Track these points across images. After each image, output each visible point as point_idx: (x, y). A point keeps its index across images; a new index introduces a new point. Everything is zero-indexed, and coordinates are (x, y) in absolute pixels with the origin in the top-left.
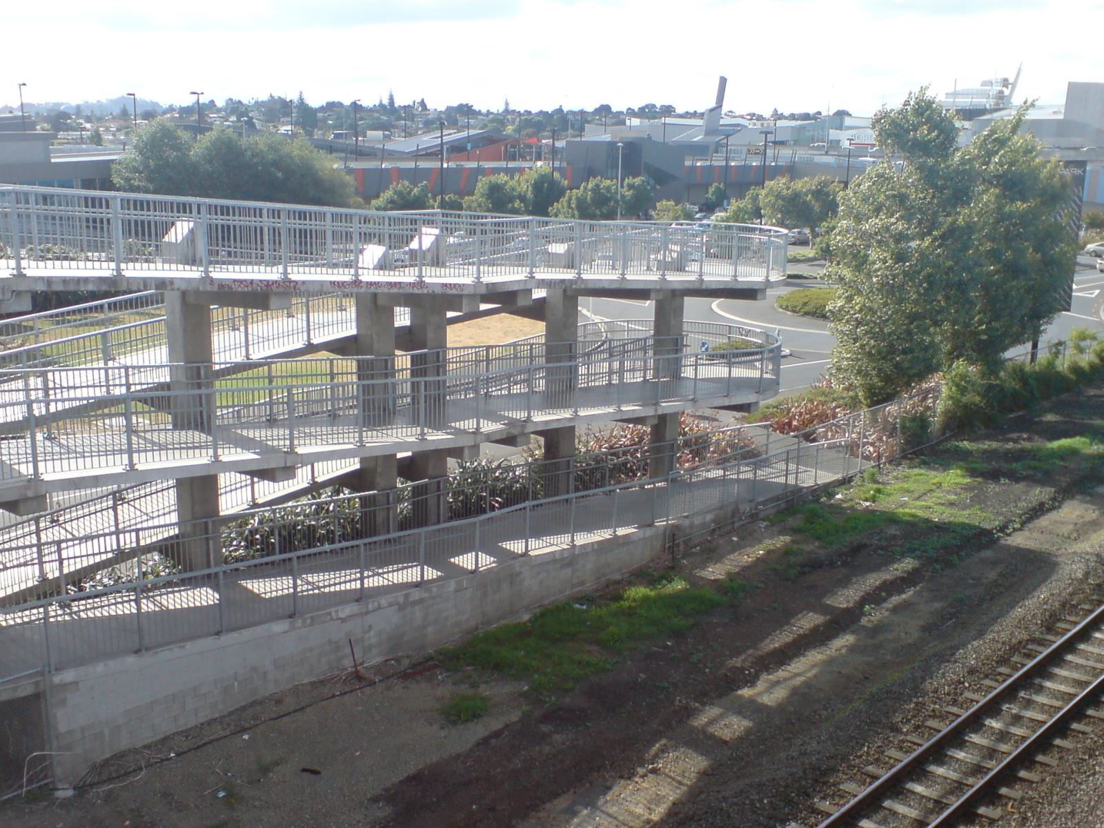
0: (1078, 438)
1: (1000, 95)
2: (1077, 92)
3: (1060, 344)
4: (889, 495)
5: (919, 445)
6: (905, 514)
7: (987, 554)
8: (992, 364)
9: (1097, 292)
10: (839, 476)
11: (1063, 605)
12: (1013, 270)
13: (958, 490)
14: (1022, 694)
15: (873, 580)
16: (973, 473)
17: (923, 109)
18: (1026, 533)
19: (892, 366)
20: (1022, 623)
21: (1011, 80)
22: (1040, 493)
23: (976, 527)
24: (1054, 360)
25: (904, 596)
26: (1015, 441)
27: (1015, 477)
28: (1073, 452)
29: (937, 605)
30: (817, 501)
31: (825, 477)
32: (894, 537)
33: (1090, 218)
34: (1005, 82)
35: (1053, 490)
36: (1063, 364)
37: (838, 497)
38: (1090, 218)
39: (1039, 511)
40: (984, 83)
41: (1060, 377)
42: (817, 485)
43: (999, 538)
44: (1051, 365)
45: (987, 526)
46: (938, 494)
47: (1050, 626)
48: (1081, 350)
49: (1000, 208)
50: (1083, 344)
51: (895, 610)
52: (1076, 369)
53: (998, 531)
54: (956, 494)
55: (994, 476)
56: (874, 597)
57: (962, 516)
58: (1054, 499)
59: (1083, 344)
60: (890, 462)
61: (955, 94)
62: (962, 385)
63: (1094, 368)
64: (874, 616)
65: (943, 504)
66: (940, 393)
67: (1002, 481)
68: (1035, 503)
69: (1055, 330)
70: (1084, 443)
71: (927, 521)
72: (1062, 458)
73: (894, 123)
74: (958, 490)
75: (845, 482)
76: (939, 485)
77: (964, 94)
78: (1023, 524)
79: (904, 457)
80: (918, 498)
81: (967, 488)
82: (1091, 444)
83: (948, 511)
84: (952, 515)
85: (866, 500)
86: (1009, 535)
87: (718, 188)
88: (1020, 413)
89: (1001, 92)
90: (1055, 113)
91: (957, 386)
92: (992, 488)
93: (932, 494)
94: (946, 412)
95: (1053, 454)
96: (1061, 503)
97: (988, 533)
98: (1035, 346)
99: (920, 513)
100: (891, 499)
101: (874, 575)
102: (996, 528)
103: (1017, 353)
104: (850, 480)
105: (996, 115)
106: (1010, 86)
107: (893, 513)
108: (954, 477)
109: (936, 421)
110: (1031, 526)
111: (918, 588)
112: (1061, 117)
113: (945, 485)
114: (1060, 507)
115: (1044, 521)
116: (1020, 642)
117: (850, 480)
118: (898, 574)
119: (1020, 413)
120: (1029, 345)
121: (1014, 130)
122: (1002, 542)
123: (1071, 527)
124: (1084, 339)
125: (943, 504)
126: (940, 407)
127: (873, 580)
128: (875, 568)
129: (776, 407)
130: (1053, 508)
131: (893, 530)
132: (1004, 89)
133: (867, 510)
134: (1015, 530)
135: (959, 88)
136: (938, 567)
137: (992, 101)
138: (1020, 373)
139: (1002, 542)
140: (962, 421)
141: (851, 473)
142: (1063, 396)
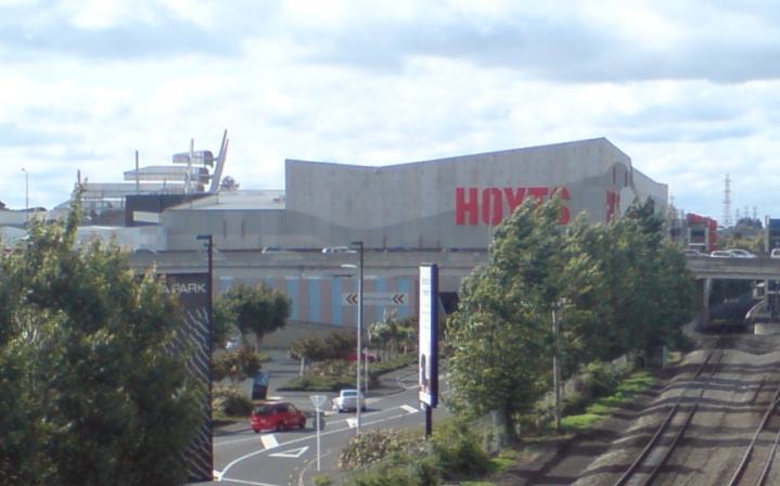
1: (204, 176)
2: (297, 171)
9: (304, 449)
17: (232, 181)
21: (216, 155)
33: (307, 347)
34: (208, 157)
38: (307, 347)
40: (178, 158)
61: (137, 174)
77: (152, 172)
87: (157, 357)
89: (204, 171)
90: (276, 200)
105: (197, 204)
106: (215, 163)
112: (282, 206)
121: (72, 225)
132: (208, 167)
135: (142, 165)
137: (194, 184)
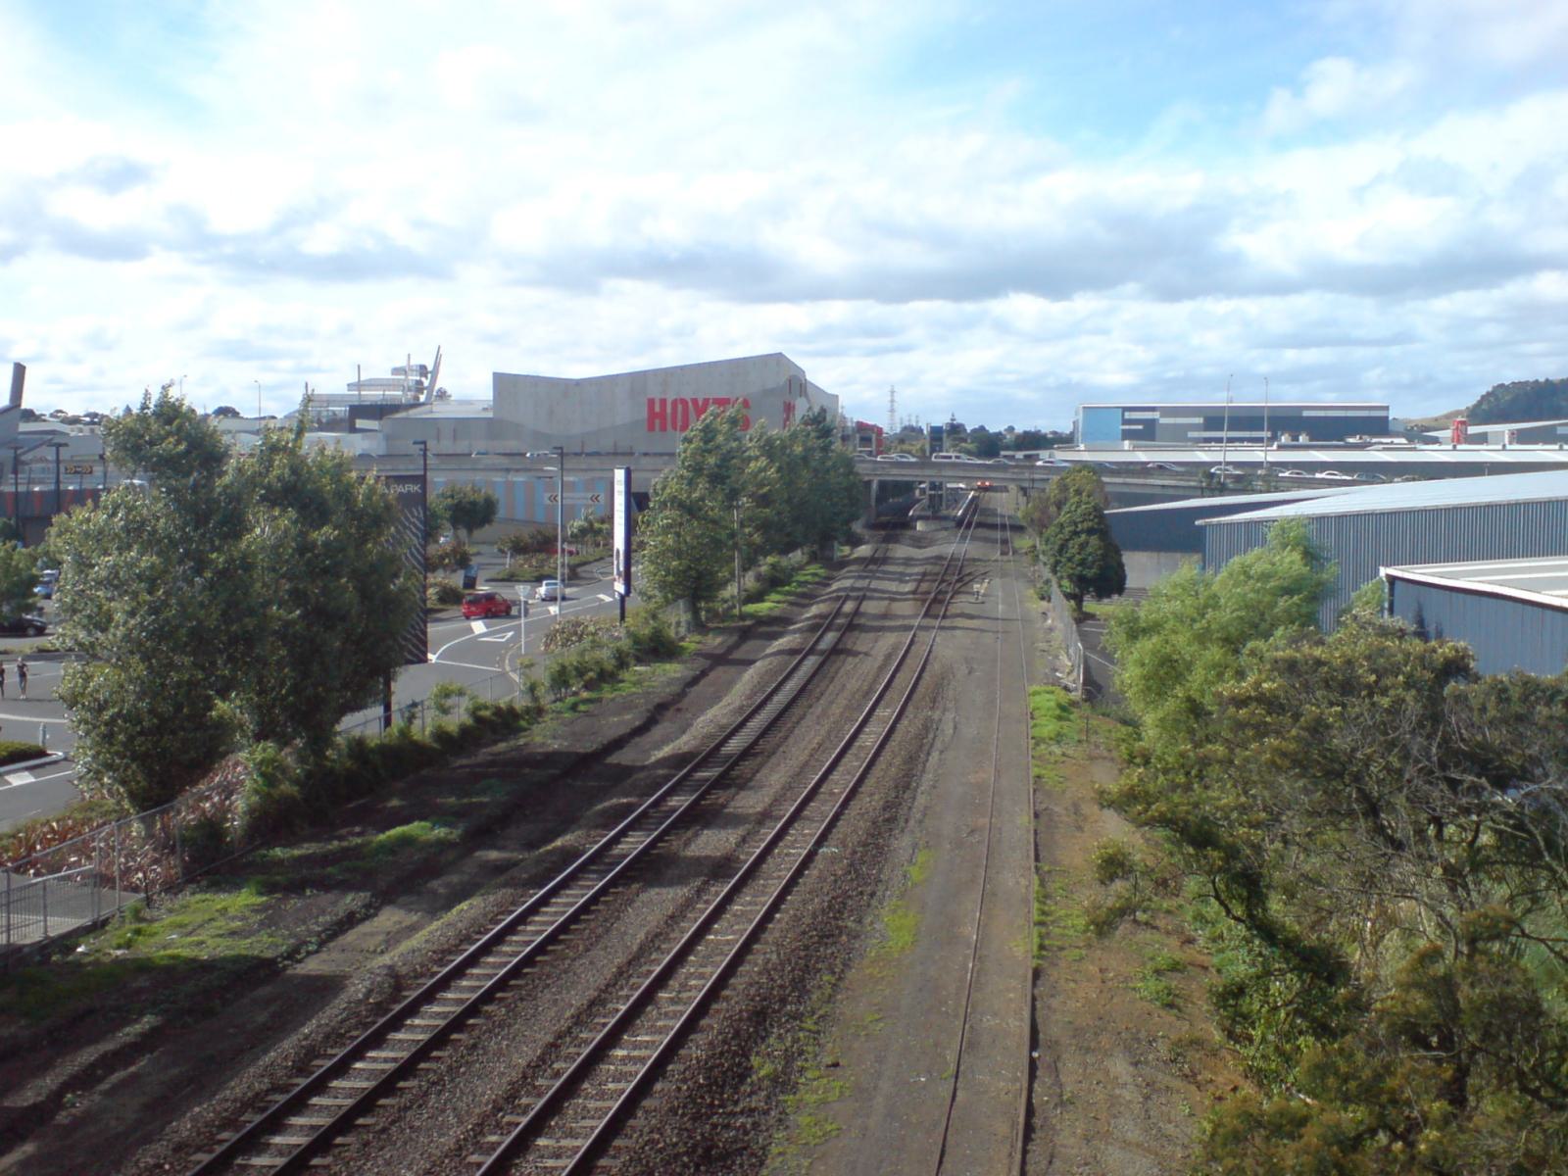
0: (416, 824)
3: (414, 705)
4: (152, 935)
5: (209, 860)
6: (162, 958)
7: (264, 991)
8: (320, 738)
9: (510, 634)
10: (86, 921)
11: (327, 1037)
12: (323, 615)
13: (247, 914)
14: (239, 1161)
15: (88, 1055)
16: (269, 888)
17: (170, 413)
18: (323, 956)
19: (158, 753)
20: (269, 1071)
21: (430, 368)
22: (352, 901)
23: (254, 958)
24: (409, 727)
25: (133, 1069)
26: (341, 838)
27: (324, 885)
28: (406, 841)
29: (175, 1071)
30: (45, 960)
31: (60, 925)
32: (140, 991)
35: (368, 894)
36: (423, 729)
37: (79, 950)
39: (350, 921)
40: (396, 371)
41: (418, 748)
42: (47, 937)
43: (285, 968)
44: (404, 734)
45: (269, 954)
46: (221, 922)
47: (301, 1069)
48: (445, 711)
49: (303, 534)
50: (449, 702)
51: (107, 1094)
52: (441, 735)
53: (285, 959)
54: (241, 920)
55: (296, 888)
56: (84, 1081)
57: (243, 947)
58: (367, 906)
59: (449, 702)
60: (167, 891)
61: (359, 385)
62: (270, 774)
63: (465, 730)
64: (78, 1104)
65: (221, 936)
66: (239, 783)
67: (308, 893)
68: (341, 914)
69: (409, 685)
70: (423, 828)
71: (194, 960)
72: (393, 852)
73: (131, 432)
74: (247, 914)
75: (98, 927)
76: (223, 911)
78: (322, 944)
79: (191, 881)
80: (190, 934)
81: (263, 908)
82: (432, 829)
83: (229, 942)
84: (228, 947)
85: (119, 947)
86: (300, 961)
88: (362, 801)
89: (420, 383)
91: (263, 775)
92: (295, 902)
93: (209, 925)
94: (251, 811)
95: (382, 847)
96: (378, 909)
97: (270, 963)
98: (388, 708)
99: (186, 953)
100: (157, 939)
101: (91, 1049)
102: (281, 956)
103: (362, 724)
104: (105, 922)
107: (149, 959)
108: (244, 899)
109: (236, 823)
110: (331, 945)
111: (155, 1054)
112: (490, 415)
113: (232, 912)
114: (376, 915)
115: (350, 937)
116: (257, 1094)
117: (105, 922)
118: (128, 1039)
119: (362, 801)
120: (379, 710)
122: (290, 972)
123: (381, 938)
124: (447, 695)
125: (221, 936)
126: (240, 803)
127: (88, 1055)
128: (94, 1040)
129: (14, 836)
130: (367, 917)
131: (142, 982)
133: (117, 961)
134: (309, 953)
136: (190, 1020)
138: (358, 747)
139: (290, 972)
140: (275, 821)
141: (105, 913)
142: (424, 772)
